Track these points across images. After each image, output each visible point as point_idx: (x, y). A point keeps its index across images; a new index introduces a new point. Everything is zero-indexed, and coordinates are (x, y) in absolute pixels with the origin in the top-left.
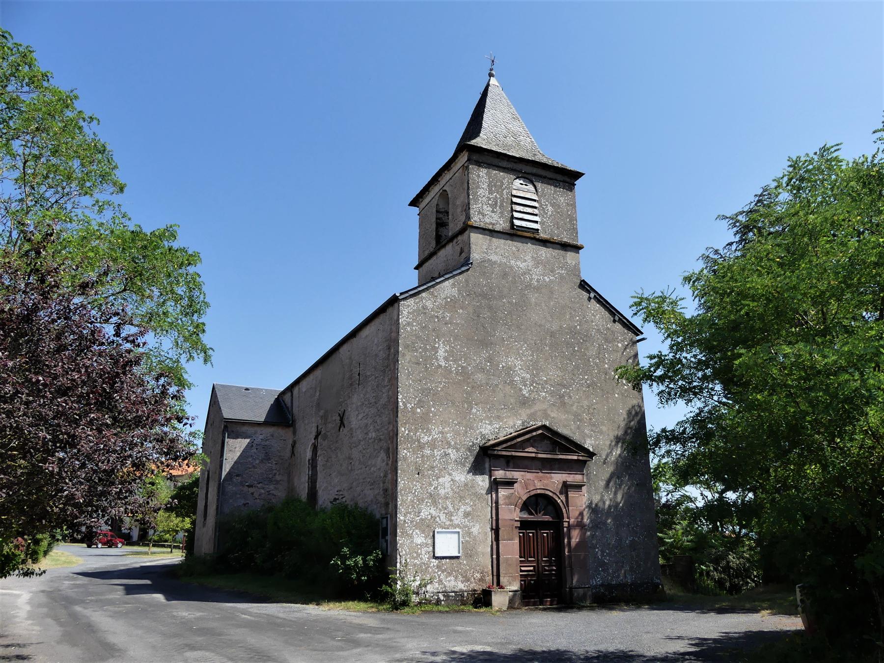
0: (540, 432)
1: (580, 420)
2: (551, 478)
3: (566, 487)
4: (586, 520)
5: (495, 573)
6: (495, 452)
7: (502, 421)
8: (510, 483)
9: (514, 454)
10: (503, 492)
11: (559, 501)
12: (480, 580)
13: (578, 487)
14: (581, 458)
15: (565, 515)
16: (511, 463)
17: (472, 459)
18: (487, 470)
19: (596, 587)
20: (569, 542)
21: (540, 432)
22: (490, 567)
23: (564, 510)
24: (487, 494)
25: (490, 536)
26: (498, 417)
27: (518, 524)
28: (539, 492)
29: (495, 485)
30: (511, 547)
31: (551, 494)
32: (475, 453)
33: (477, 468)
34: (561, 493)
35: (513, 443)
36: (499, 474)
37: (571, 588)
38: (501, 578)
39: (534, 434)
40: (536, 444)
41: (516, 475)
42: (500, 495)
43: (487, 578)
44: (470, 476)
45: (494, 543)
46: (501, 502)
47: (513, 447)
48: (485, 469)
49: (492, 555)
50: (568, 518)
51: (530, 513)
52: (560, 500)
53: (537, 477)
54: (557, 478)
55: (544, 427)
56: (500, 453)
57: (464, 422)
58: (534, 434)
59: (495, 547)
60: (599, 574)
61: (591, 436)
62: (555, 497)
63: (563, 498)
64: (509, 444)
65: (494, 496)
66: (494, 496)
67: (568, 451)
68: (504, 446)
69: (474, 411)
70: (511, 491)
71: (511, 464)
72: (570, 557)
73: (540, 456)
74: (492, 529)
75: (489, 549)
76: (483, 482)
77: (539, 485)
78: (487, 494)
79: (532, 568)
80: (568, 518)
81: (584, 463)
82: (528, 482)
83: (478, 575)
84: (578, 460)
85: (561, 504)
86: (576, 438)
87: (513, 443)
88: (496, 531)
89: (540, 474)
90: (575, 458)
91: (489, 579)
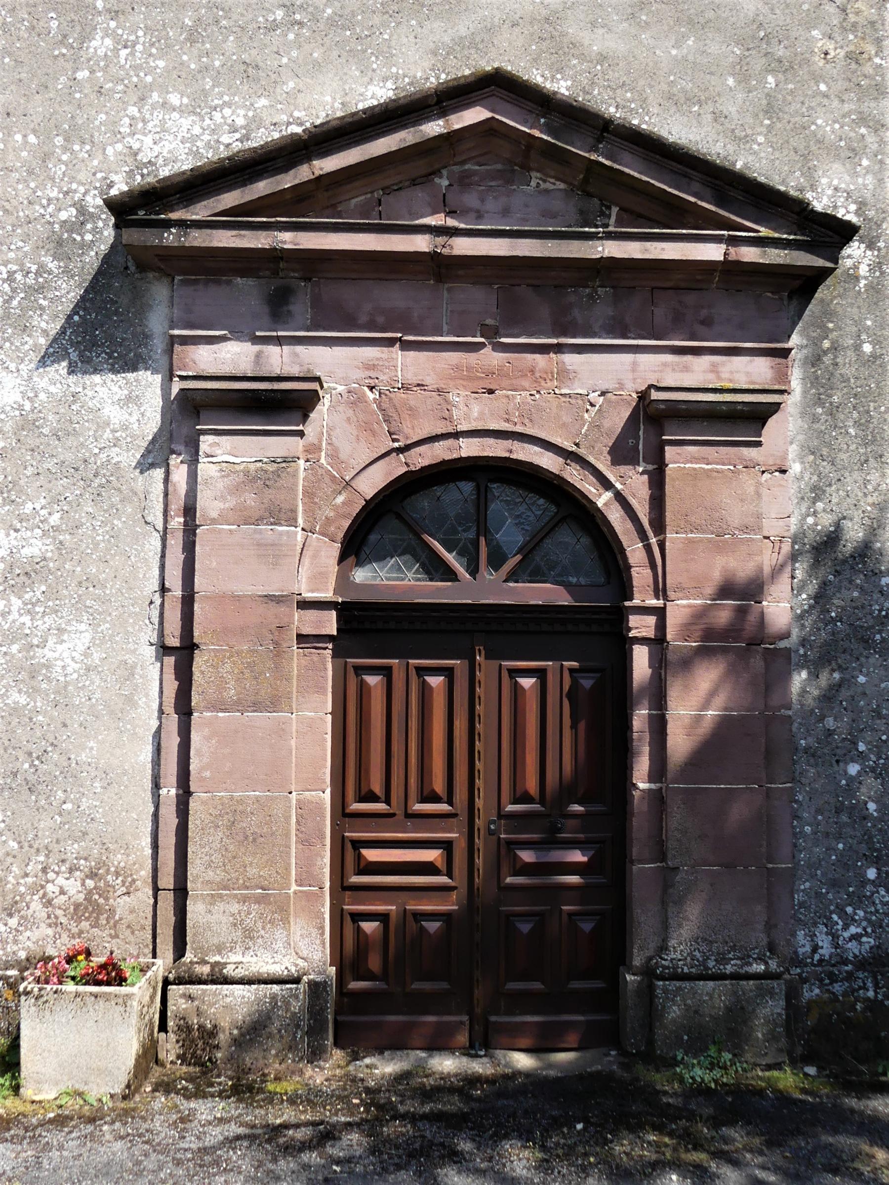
0: (474, 115)
1: (784, 67)
2: (563, 375)
3: (655, 423)
4: (780, 608)
5: (167, 880)
6: (170, 237)
7: (266, 91)
8: (280, 405)
9: (288, 240)
10: (226, 453)
11: (603, 499)
12: (78, 911)
13: (745, 419)
14: (749, 254)
15: (641, 576)
16: (290, 291)
17: (68, 292)
18: (158, 345)
19: (829, 969)
20: (659, 726)
21: (474, 115)
22: (146, 841)
23: (635, 553)
24: (144, 466)
25: (152, 678)
26: (249, 71)
27: (329, 623)
28: (469, 448)
29: (198, 410)
30: (285, 746)
31: (548, 461)
32: (92, 259)
33: (99, 334)
34: (622, 453)
35: (287, 181)
36: (227, 357)
37: (649, 973)
38: (195, 910)
39: (434, 128)
40: (471, 199)
41: (336, 365)
42: (205, 468)
43: (122, 904)
44: (56, 379)
45: (173, 721)
46: (209, 504)
47: (296, 206)
48: (145, 338)
49: (156, 786)
50: (660, 590)
51: (437, 569)
52: (616, 493)
53: (466, 376)
54: (596, 382)
55: (497, 85)
56: (198, 239)
57: (38, 108)
58: (434, 128)
59: (172, 742)
60: (858, 900)
61: (854, 153)
62: (574, 475)
63: (635, 482)
64: (262, 188)
65: (180, 475)
66: (180, 475)
67: (674, 217)
68: (230, 199)
69: (100, 45)
70: (278, 446)
71: (300, 307)
72: (658, 799)
73: (463, 246)
74: (164, 650)
75: (146, 754)
76: (128, 404)
77: (471, 411)
78: (144, 466)
79: (372, 855)
80: (660, 590)
81: (802, 286)
82: (379, 399)
83: (74, 887)
84: (730, 270)
85: (616, 517)
86: (758, 159)
87: (287, 181)
88: (181, 654)
89: (490, 357)
90: (713, 252)
91: (134, 904)
